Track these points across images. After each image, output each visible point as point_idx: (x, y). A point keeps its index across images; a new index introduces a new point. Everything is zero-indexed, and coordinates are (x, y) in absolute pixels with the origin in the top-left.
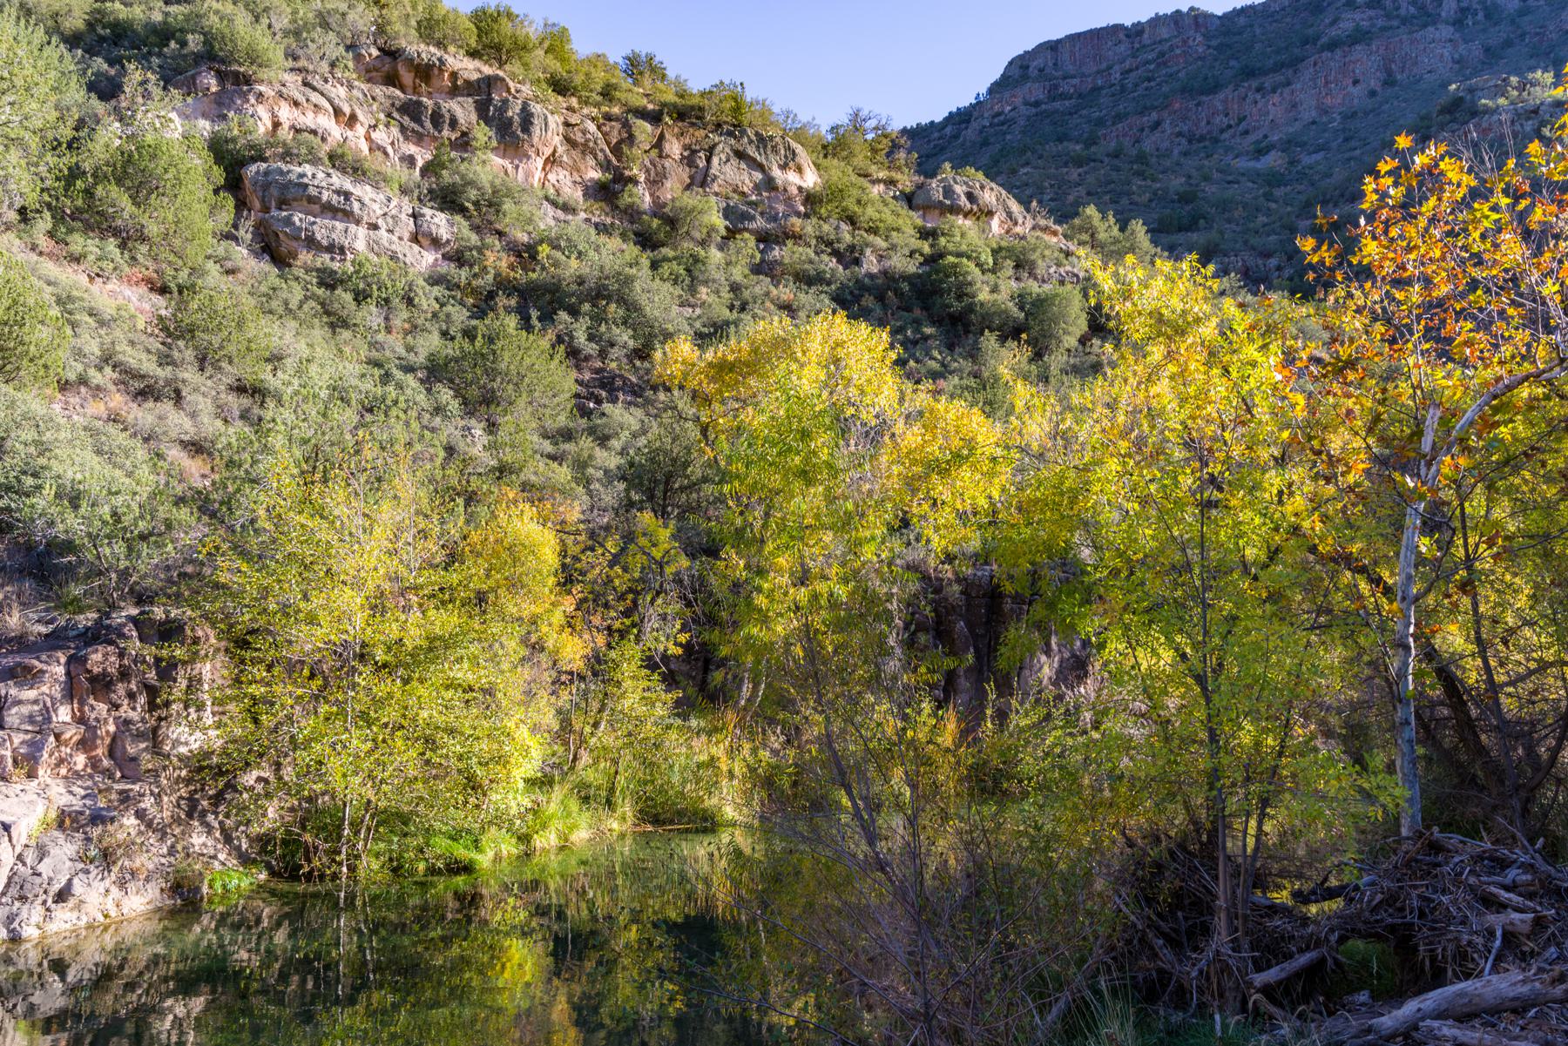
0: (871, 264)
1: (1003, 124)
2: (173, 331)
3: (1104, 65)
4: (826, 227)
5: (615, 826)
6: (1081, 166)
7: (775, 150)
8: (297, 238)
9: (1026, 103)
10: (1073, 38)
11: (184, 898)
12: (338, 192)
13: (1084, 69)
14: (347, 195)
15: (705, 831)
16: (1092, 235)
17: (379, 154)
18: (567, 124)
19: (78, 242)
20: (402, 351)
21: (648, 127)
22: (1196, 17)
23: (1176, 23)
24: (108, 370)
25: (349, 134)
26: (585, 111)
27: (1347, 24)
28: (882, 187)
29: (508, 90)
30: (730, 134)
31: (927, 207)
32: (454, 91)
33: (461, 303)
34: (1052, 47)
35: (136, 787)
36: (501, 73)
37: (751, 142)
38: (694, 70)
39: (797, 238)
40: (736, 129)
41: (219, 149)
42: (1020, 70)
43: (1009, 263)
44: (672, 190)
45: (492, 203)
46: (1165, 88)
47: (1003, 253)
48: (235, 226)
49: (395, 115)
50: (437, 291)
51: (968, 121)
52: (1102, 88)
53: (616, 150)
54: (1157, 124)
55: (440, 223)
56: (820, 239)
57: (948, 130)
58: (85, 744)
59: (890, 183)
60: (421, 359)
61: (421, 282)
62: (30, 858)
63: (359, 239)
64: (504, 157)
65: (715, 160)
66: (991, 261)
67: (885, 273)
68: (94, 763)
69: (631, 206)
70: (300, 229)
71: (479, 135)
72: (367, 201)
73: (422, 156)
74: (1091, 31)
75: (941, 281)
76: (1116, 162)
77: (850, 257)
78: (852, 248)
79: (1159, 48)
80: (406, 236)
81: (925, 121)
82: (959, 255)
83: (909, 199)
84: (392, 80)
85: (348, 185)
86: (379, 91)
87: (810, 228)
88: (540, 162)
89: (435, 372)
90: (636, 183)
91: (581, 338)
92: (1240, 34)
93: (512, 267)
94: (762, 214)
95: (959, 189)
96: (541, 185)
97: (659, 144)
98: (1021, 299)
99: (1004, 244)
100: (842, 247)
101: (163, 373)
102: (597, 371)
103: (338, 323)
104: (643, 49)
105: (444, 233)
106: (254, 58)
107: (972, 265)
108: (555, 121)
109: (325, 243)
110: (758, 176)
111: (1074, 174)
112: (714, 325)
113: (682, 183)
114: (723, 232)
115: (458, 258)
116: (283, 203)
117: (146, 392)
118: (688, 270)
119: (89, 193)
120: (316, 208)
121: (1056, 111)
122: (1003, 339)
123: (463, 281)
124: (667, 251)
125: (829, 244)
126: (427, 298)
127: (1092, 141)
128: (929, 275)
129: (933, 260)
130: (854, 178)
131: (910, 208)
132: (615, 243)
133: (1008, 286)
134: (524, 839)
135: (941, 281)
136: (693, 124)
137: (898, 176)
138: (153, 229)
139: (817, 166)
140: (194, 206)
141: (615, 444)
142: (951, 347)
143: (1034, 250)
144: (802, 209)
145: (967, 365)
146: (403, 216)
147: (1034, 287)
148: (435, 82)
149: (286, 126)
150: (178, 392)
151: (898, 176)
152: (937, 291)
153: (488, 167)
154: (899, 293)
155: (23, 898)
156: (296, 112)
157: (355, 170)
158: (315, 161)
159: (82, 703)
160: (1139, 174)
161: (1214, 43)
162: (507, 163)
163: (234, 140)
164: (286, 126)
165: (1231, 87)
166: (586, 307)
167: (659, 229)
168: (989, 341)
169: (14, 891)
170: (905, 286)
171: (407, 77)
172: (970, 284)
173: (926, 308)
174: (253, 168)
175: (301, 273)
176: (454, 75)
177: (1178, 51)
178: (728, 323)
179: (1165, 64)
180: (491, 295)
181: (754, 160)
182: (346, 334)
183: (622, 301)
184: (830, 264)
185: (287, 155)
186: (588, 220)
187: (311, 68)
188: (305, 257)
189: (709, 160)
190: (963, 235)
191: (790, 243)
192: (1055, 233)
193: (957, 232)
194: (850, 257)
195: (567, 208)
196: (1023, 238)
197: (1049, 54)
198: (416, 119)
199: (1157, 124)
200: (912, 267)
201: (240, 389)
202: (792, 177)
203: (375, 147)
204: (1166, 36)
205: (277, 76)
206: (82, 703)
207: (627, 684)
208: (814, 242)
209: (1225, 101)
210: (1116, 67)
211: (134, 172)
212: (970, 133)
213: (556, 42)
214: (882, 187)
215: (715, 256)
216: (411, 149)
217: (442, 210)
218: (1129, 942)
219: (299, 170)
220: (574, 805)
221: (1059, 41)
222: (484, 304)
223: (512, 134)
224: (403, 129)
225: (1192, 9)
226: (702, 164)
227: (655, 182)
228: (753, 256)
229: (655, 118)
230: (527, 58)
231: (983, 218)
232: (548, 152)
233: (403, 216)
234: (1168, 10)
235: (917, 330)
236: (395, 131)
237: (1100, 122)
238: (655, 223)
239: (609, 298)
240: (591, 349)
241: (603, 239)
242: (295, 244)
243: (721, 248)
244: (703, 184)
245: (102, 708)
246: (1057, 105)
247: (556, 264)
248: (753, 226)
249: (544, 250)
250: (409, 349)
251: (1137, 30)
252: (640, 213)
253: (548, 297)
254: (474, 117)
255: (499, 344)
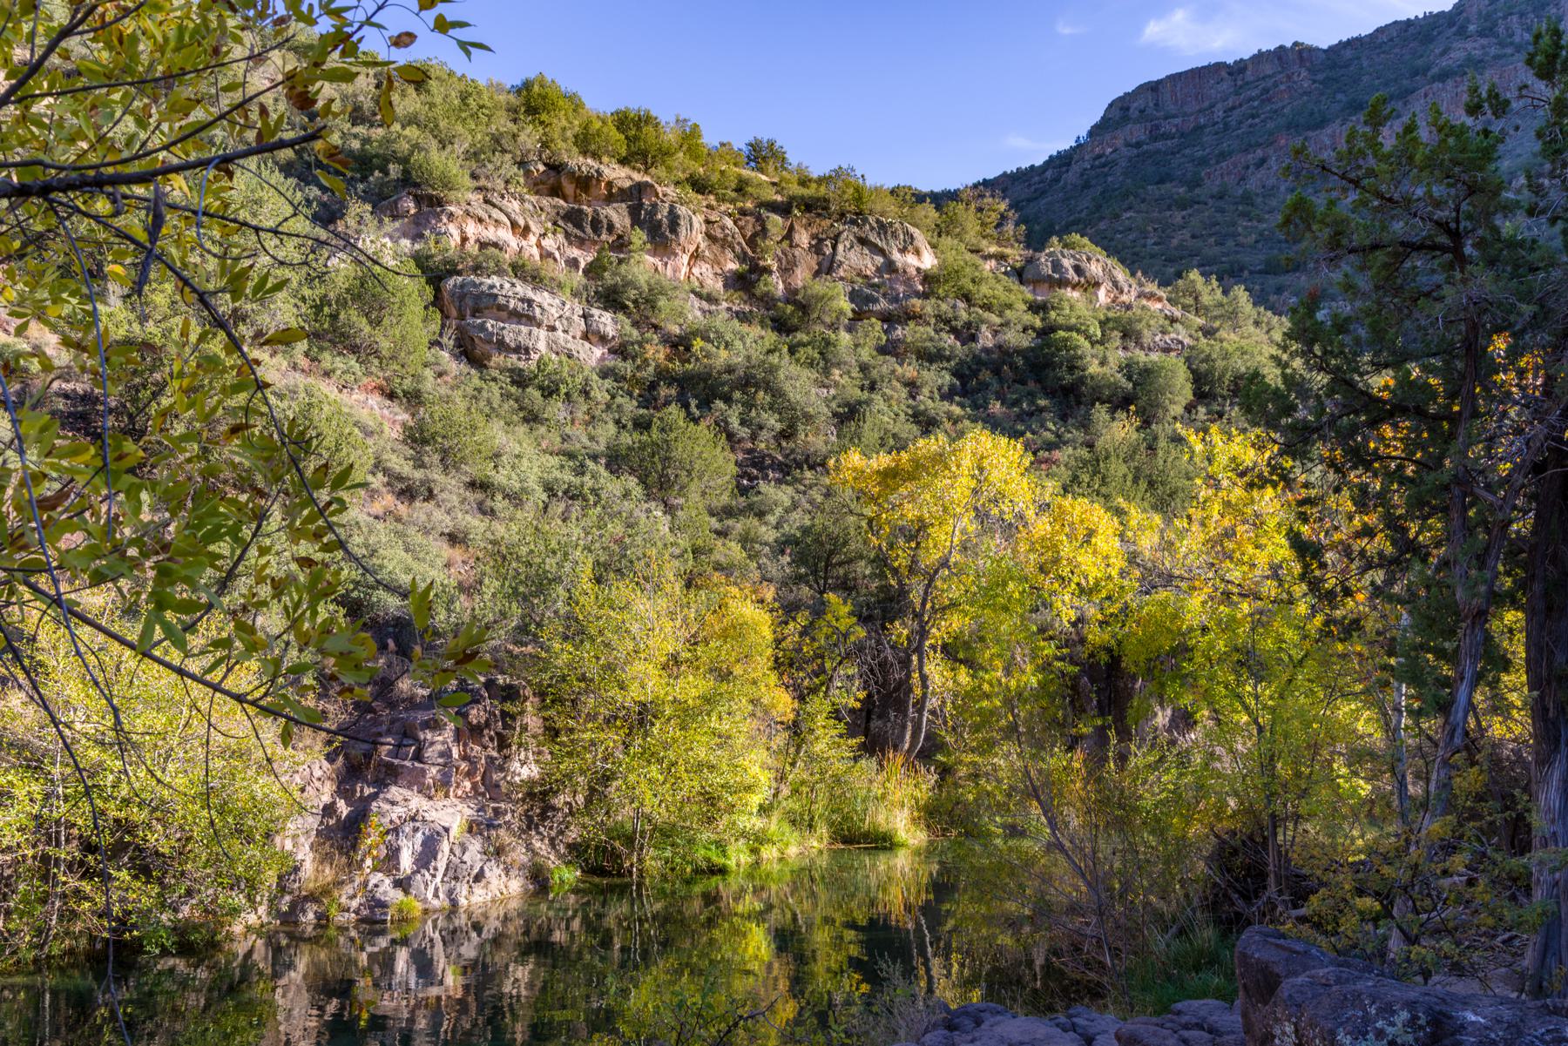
0: (986, 339)
1: (1104, 166)
2: (417, 438)
3: (1206, 104)
4: (944, 307)
5: (815, 844)
6: (1184, 209)
7: (895, 235)
8: (490, 342)
9: (1128, 145)
10: (1174, 78)
11: (539, 879)
12: (522, 300)
13: (1186, 109)
14: (530, 302)
15: (885, 849)
16: (1196, 299)
17: (551, 261)
18: (708, 222)
19: (327, 359)
20: (585, 440)
21: (777, 219)
22: (1300, 52)
23: (1280, 58)
24: (380, 475)
25: (524, 243)
26: (723, 208)
27: (1457, 55)
28: (993, 262)
29: (657, 195)
30: (853, 222)
31: (1037, 281)
32: (610, 199)
33: (630, 394)
34: (1153, 88)
35: (502, 805)
36: (647, 179)
37: (872, 229)
38: (812, 155)
39: (916, 317)
40: (858, 217)
41: (420, 260)
42: (1120, 112)
43: (1117, 334)
44: (801, 276)
45: (649, 301)
46: (1270, 125)
47: (1111, 325)
48: (441, 335)
49: (560, 223)
50: (608, 383)
51: (1069, 164)
52: (1205, 126)
53: (751, 242)
54: (1263, 161)
55: (606, 321)
56: (938, 317)
57: (1049, 174)
58: (469, 774)
59: (1001, 257)
60: (601, 448)
61: (595, 377)
62: (458, 851)
63: (540, 340)
64: (654, 256)
65: (840, 248)
66: (1099, 333)
67: (1000, 347)
68: (474, 787)
69: (767, 294)
70: (492, 334)
71: (635, 240)
72: (546, 306)
73: (585, 258)
74: (1192, 70)
75: (1053, 355)
76: (1221, 203)
77: (967, 334)
78: (968, 325)
79: (1263, 85)
80: (579, 334)
81: (1025, 165)
82: (1069, 329)
83: (1019, 274)
84: (555, 191)
85: (530, 294)
86: (546, 202)
87: (929, 307)
88: (686, 258)
89: (615, 461)
90: (770, 272)
91: (735, 422)
92: (1346, 66)
93: (669, 359)
94: (884, 295)
95: (1067, 263)
96: (687, 276)
97: (789, 235)
98: (1128, 368)
99: (1111, 315)
100: (959, 324)
101: (418, 475)
102: (750, 451)
103: (532, 418)
104: (765, 136)
105: (610, 331)
106: (448, 185)
107: (1081, 340)
108: (698, 220)
109: (513, 345)
110: (880, 260)
111: (1178, 217)
112: (847, 404)
113: (810, 269)
114: (850, 315)
115: (621, 351)
116: (476, 312)
117: (408, 493)
118: (821, 353)
119: (334, 317)
120: (504, 314)
121: (1158, 151)
122: (1112, 411)
123: (629, 374)
124: (801, 336)
125: (947, 322)
126: (600, 394)
127: (1195, 183)
128: (1041, 348)
129: (1046, 331)
130: (968, 256)
131: (1021, 283)
132: (755, 331)
133: (1116, 356)
134: (754, 851)
135: (1053, 355)
136: (819, 215)
137: (1008, 251)
138: (385, 345)
139: (934, 246)
140: (412, 320)
141: (772, 519)
142: (1064, 418)
143: (1140, 321)
144: (920, 288)
145: (1079, 435)
146: (576, 318)
147: (1141, 356)
148: (593, 191)
149: (472, 241)
150: (430, 491)
151: (1008, 251)
152: (1049, 364)
153: (644, 266)
154: (1013, 366)
155: (456, 878)
156: (480, 228)
157: (534, 278)
158: (500, 272)
159: (465, 745)
160: (1244, 215)
161: (1320, 77)
162: (656, 261)
163: (432, 256)
164: (472, 241)
165: (1338, 121)
166: (737, 395)
167: (793, 313)
168: (1100, 413)
169: (451, 874)
170: (1020, 362)
171: (569, 188)
172: (1081, 358)
173: (1038, 381)
174: (451, 282)
175: (495, 373)
176: (610, 184)
177: (1282, 87)
178: (860, 403)
179: (1269, 100)
180: (653, 386)
181: (876, 246)
182: (543, 430)
183: (767, 387)
184: (949, 340)
185: (477, 268)
186: (729, 309)
187: (489, 185)
188: (497, 359)
189: (834, 247)
190: (1072, 308)
191: (912, 324)
192: (1160, 300)
193: (1066, 305)
194: (967, 334)
195: (710, 299)
196: (1129, 307)
197: (1149, 95)
198: (579, 226)
199: (1263, 161)
200: (1025, 341)
201: (472, 485)
202: (911, 259)
203: (546, 255)
204: (1269, 72)
205: (465, 196)
206: (465, 745)
207: (820, 732)
208: (933, 321)
209: (1333, 136)
210: (1219, 106)
211: (369, 293)
212: (1071, 176)
213: (690, 137)
214: (993, 262)
215: (845, 338)
216: (575, 252)
217: (605, 309)
218: (1216, 895)
219: (489, 281)
220: (787, 828)
221: (1159, 82)
222: (649, 397)
223: (662, 235)
224: (567, 235)
225: (1296, 44)
226: (828, 251)
227: (787, 269)
228: (879, 338)
229: (784, 210)
230: (669, 161)
231: (1091, 289)
232: (692, 248)
233: (576, 318)
234: (1270, 45)
235: (1032, 403)
236: (561, 237)
237: (1203, 162)
238: (790, 308)
239: (757, 386)
240: (744, 432)
241: (745, 328)
242: (487, 347)
243: (849, 330)
244: (829, 271)
245: (478, 748)
246: (1159, 145)
247: (708, 356)
248: (877, 307)
249: (698, 344)
250: (592, 438)
251: (1240, 67)
252: (773, 299)
253: (702, 385)
254: (628, 221)
255: (673, 435)
